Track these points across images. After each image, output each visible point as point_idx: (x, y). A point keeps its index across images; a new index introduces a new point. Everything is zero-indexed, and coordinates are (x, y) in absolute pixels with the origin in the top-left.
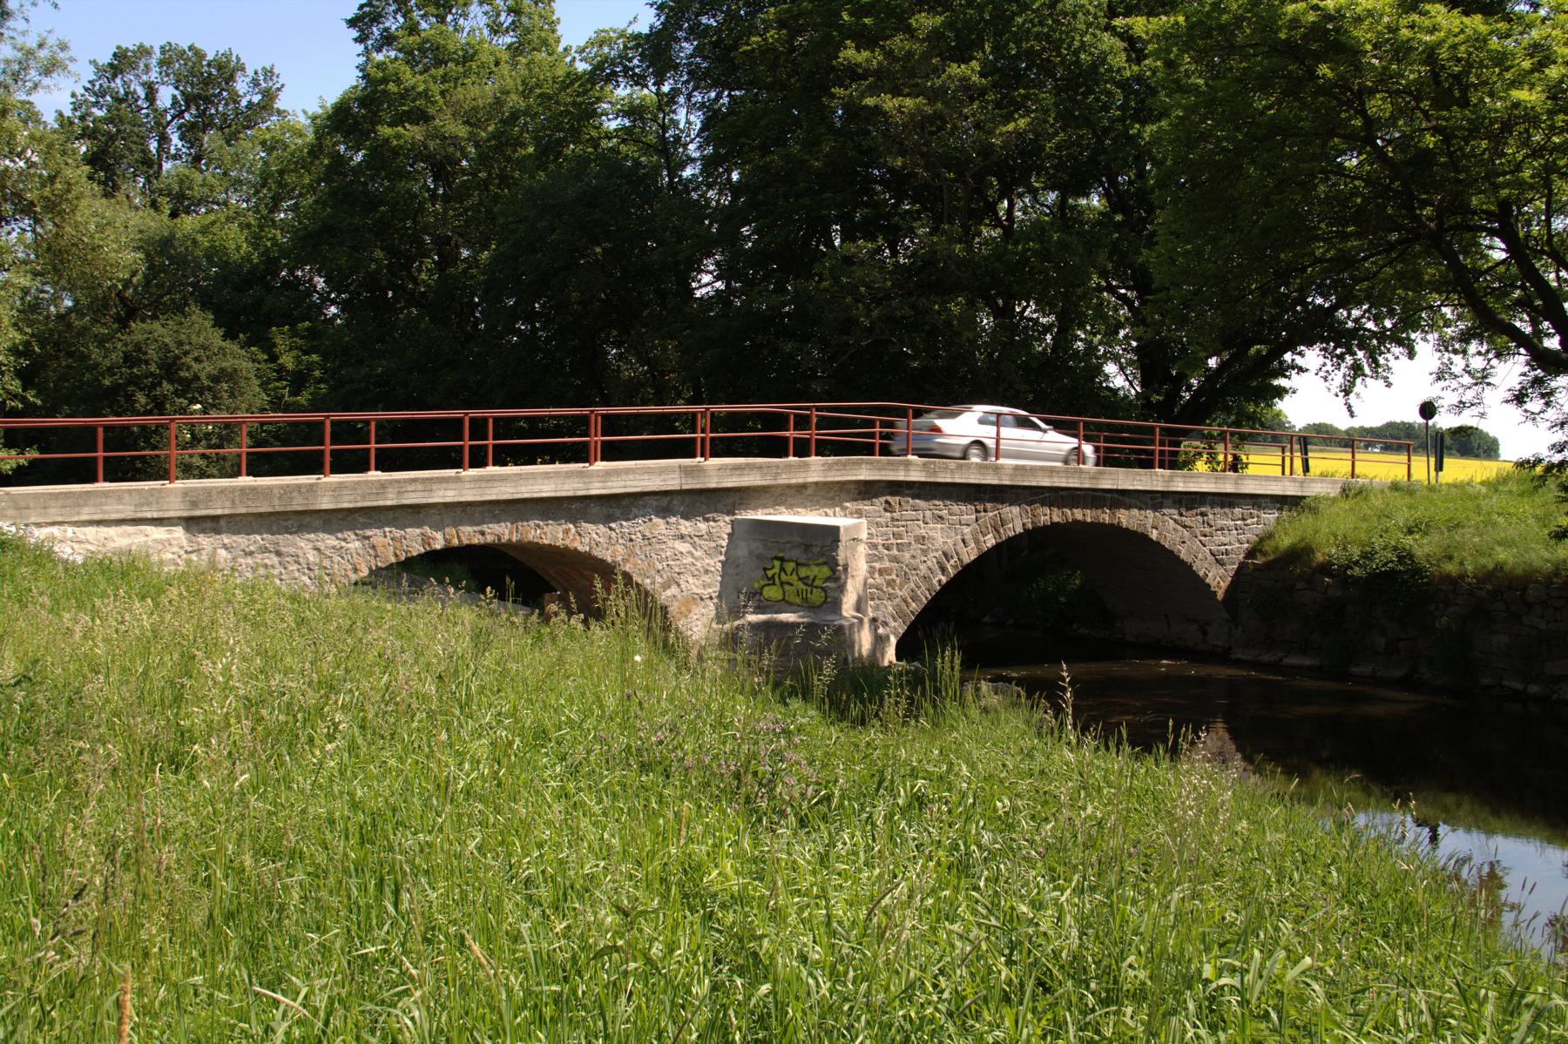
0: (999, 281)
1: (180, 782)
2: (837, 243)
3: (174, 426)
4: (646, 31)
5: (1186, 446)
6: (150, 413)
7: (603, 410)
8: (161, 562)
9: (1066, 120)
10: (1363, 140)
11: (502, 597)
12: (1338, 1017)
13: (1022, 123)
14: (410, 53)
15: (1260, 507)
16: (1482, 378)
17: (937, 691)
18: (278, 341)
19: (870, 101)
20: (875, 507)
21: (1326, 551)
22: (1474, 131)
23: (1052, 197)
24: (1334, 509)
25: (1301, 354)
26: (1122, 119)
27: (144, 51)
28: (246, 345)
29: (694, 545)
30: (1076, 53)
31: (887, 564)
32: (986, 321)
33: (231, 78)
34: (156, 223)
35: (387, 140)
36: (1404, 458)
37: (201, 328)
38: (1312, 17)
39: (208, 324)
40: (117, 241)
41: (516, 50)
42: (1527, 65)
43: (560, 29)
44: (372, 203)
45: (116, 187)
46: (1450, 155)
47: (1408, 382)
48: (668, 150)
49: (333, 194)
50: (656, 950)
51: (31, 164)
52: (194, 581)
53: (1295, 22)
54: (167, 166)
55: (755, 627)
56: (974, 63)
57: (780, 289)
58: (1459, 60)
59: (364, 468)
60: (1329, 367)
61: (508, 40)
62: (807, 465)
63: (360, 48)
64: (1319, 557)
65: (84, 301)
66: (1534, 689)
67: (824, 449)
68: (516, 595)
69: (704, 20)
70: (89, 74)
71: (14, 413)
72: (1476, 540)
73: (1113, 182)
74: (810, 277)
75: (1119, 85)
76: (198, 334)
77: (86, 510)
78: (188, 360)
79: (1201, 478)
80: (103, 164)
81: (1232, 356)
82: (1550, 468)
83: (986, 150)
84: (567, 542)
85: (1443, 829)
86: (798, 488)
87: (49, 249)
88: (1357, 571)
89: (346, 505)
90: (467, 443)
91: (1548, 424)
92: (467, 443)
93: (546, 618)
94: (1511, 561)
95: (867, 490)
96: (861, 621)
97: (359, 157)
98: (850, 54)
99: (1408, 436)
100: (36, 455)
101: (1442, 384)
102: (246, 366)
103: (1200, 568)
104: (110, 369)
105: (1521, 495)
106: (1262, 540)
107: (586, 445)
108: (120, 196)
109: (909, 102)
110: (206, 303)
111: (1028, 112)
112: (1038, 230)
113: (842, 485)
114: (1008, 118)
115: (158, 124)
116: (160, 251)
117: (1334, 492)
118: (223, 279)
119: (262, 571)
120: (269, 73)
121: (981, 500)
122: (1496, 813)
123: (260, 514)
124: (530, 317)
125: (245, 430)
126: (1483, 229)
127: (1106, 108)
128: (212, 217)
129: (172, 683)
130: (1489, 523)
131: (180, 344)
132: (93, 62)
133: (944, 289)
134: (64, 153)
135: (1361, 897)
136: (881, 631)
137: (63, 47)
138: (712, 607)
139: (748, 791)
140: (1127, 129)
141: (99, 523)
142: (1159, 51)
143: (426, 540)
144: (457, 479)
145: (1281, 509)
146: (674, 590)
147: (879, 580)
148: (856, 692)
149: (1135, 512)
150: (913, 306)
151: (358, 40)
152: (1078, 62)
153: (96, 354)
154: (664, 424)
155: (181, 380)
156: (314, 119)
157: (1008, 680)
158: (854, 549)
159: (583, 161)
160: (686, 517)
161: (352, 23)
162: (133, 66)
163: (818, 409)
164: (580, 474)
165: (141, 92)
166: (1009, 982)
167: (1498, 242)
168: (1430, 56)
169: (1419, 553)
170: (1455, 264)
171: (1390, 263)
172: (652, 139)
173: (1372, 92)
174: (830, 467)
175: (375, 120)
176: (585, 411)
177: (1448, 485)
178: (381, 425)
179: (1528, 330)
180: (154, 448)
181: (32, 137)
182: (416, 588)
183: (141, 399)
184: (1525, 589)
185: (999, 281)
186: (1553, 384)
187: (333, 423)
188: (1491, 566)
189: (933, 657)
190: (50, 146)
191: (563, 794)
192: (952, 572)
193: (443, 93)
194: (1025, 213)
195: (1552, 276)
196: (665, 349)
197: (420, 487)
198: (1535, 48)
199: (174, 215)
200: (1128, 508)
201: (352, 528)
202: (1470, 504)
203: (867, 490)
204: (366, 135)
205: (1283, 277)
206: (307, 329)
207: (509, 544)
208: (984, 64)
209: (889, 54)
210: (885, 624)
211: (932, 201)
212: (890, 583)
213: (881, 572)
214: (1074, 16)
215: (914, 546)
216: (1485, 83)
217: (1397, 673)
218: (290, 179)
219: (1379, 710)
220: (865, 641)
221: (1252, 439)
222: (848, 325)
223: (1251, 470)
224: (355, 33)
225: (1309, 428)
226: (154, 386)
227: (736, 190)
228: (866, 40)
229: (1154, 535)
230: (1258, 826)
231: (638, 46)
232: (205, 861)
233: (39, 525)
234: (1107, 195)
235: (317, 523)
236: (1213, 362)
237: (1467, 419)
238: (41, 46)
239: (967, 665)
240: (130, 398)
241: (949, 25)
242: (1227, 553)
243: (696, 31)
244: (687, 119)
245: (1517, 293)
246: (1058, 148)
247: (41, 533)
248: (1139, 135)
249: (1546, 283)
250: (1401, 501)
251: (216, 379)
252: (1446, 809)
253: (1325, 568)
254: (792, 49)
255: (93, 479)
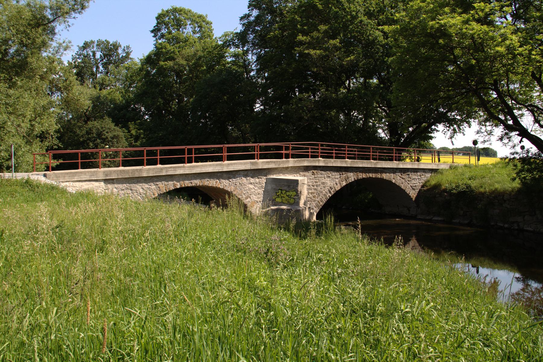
0: (345, 105)
1: (103, 256)
2: (297, 94)
3: (100, 152)
4: (239, 32)
5: (404, 154)
6: (94, 148)
7: (227, 146)
8: (97, 193)
9: (365, 56)
10: (454, 62)
11: (197, 202)
12: (441, 320)
13: (352, 57)
14: (169, 40)
15: (425, 172)
16: (490, 133)
17: (327, 228)
18: (131, 126)
19: (306, 52)
20: (309, 173)
21: (445, 185)
22: (485, 60)
23: (362, 80)
24: (448, 173)
25: (437, 126)
26: (382, 56)
27: (92, 42)
28: (121, 128)
29: (255, 186)
30: (368, 36)
31: (313, 191)
32: (342, 117)
33: (117, 49)
34: (95, 92)
35: (162, 66)
36: (468, 157)
37: (109, 123)
38: (437, 26)
39: (110, 122)
40: (84, 98)
41: (200, 38)
42: (500, 40)
43: (214, 32)
44: (158, 85)
45: (84, 82)
46: (479, 66)
47: (470, 134)
48: (246, 67)
49: (146, 82)
50: (240, 303)
51: (60, 76)
52: (106, 197)
53: (432, 27)
54: (98, 75)
55: (272, 210)
56: (337, 40)
57: (280, 108)
58: (481, 38)
59: (156, 164)
60: (446, 130)
61: (198, 35)
62: (288, 161)
63: (155, 39)
64: (443, 187)
65: (75, 116)
66: (506, 226)
67: (294, 156)
68: (202, 201)
69: (256, 28)
70: (77, 49)
71: (56, 149)
72: (489, 181)
73: (380, 75)
74: (289, 104)
75: (381, 46)
76: (107, 125)
77: (76, 177)
78: (105, 132)
79: (408, 164)
80: (80, 75)
81: (417, 127)
82: (510, 159)
83: (342, 66)
84: (217, 185)
85: (481, 269)
86: (286, 169)
87: (65, 101)
88: (454, 191)
89: (151, 175)
90: (186, 156)
91: (510, 147)
92: (186, 156)
93: (210, 208)
94: (499, 187)
95: (307, 169)
96: (305, 208)
97: (154, 71)
98: (300, 37)
99: (470, 151)
100: (62, 161)
101: (478, 135)
102: (121, 134)
103: (408, 191)
104: (82, 136)
105: (503, 168)
106: (426, 182)
107: (222, 156)
108: (85, 84)
109: (318, 52)
110: (110, 115)
111: (354, 54)
112: (357, 90)
113: (299, 168)
114: (348, 56)
115: (96, 63)
116: (97, 102)
117: (447, 167)
118: (115, 108)
119: (126, 195)
120: (128, 47)
121: (341, 171)
122: (495, 263)
123: (126, 178)
124: (205, 118)
125: (121, 153)
126: (490, 88)
127: (377, 53)
128: (112, 90)
129: (101, 228)
130: (493, 176)
131: (102, 128)
132: (78, 46)
133: (330, 108)
134: (70, 72)
135: (452, 287)
136: (311, 211)
137: (70, 42)
138: (261, 205)
139: (269, 257)
140: (384, 59)
141: (79, 181)
142: (392, 36)
143: (174, 185)
144: (184, 167)
145: (431, 173)
146: (249, 199)
147: (311, 196)
148: (302, 228)
149: (388, 174)
150: (320, 113)
151: (154, 36)
152: (369, 39)
153: (78, 132)
154: (246, 149)
155: (102, 139)
156: (141, 60)
157: (349, 225)
158: (303, 186)
159: (221, 71)
160: (252, 177)
161: (152, 31)
162: (89, 46)
163: (292, 144)
164: (220, 165)
165: (91, 54)
166: (343, 311)
167: (494, 93)
168: (472, 37)
169: (472, 185)
170: (480, 98)
171: (462, 99)
172: (242, 64)
173: (456, 48)
174: (295, 162)
175: (159, 60)
176: (222, 146)
177: (481, 165)
178: (161, 151)
179: (503, 118)
180: (95, 159)
181: (61, 68)
182: (172, 199)
183: (91, 144)
184: (504, 196)
185: (345, 105)
186: (511, 134)
187: (147, 151)
188: (494, 189)
189: (325, 218)
190: (65, 71)
191: (214, 259)
192: (333, 193)
193: (179, 52)
194: (354, 85)
195: (510, 102)
196: (246, 127)
197: (173, 169)
198: (502, 35)
199: (100, 90)
200: (386, 173)
201: (153, 182)
202: (487, 171)
203: (307, 169)
204: (156, 64)
205: (431, 102)
206: (139, 123)
207: (199, 186)
208: (340, 40)
209: (312, 37)
210: (313, 209)
211: (325, 80)
212: (314, 197)
213: (311, 193)
214: (367, 26)
215: (321, 185)
216: (488, 45)
217: (466, 222)
218: (134, 78)
219: (461, 233)
220: (307, 214)
221: (424, 152)
222: (301, 119)
223: (422, 161)
224: (153, 34)
225: (440, 148)
226: (95, 140)
227: (267, 79)
228: (305, 33)
229: (394, 181)
230: (421, 266)
231: (237, 36)
232: (110, 277)
233: (63, 182)
234: (378, 79)
235: (143, 180)
236: (411, 129)
237: (486, 145)
238: (64, 42)
239: (335, 221)
240: (88, 144)
241: (330, 28)
242: (416, 186)
243: (254, 31)
244: (251, 58)
245: (500, 107)
246: (363, 65)
247: (63, 185)
248: (387, 61)
249: (508, 105)
250: (467, 170)
251: (113, 138)
252: (481, 262)
253: (445, 190)
254: (283, 36)
255: (78, 168)
